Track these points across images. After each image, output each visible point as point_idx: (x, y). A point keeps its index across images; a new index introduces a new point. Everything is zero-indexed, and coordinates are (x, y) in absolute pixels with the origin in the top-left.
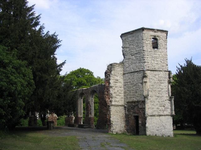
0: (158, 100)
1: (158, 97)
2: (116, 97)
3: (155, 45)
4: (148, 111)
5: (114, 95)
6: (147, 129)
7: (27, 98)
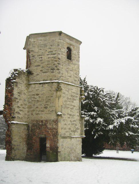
0: (70, 119)
1: (71, 115)
2: (19, 113)
3: (69, 56)
4: (61, 132)
5: (17, 110)
6: (59, 154)
7: (13, 87)
